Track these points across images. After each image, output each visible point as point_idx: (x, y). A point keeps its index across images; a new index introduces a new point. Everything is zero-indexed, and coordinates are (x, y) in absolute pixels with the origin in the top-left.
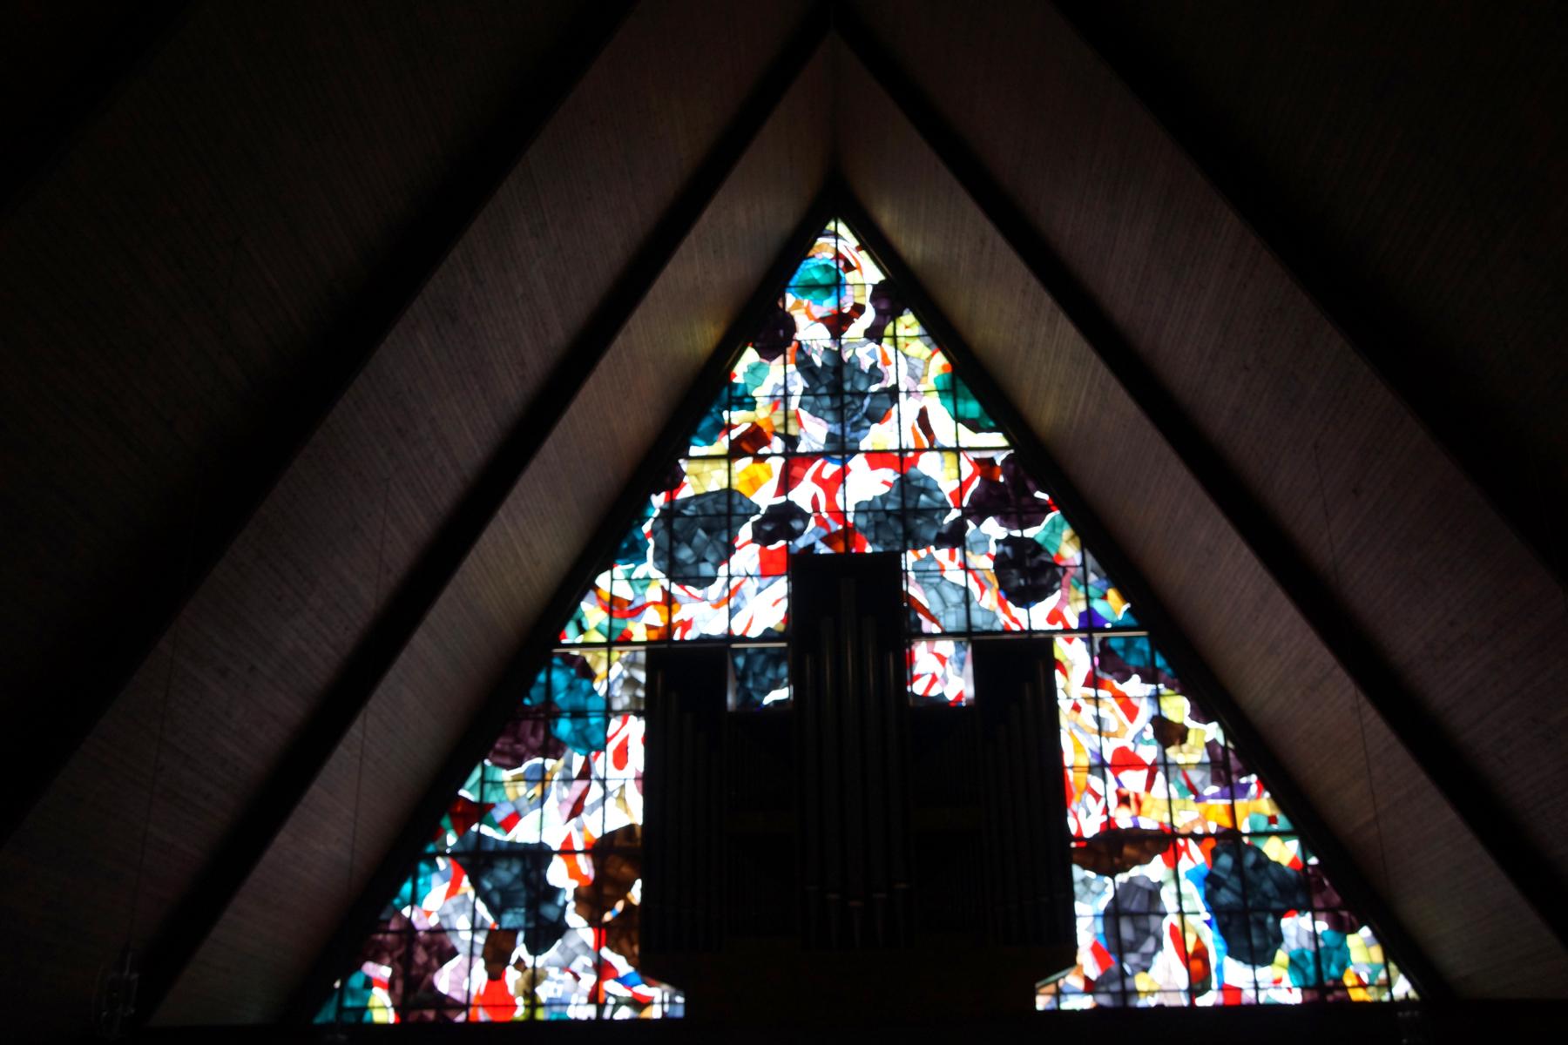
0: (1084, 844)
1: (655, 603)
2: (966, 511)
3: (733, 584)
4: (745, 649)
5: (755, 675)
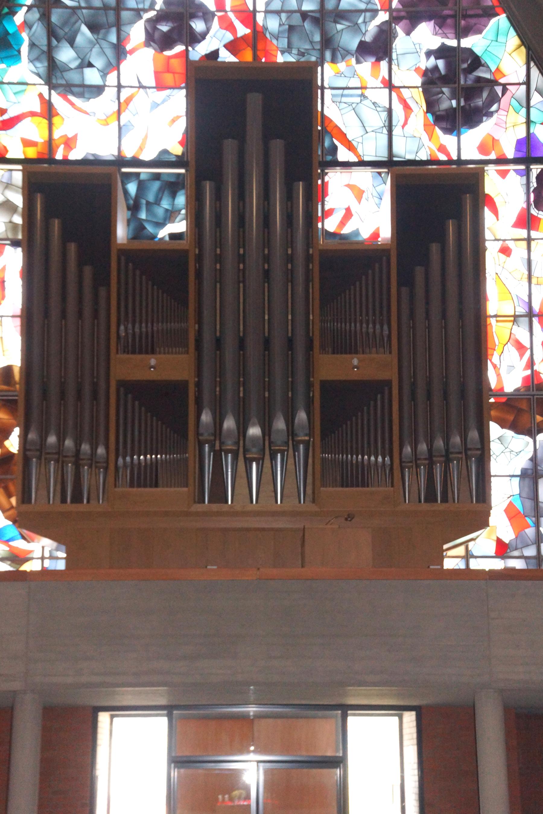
0: (503, 400)
1: (33, 114)
2: (394, 14)
3: (125, 94)
4: (138, 175)
5: (148, 203)
